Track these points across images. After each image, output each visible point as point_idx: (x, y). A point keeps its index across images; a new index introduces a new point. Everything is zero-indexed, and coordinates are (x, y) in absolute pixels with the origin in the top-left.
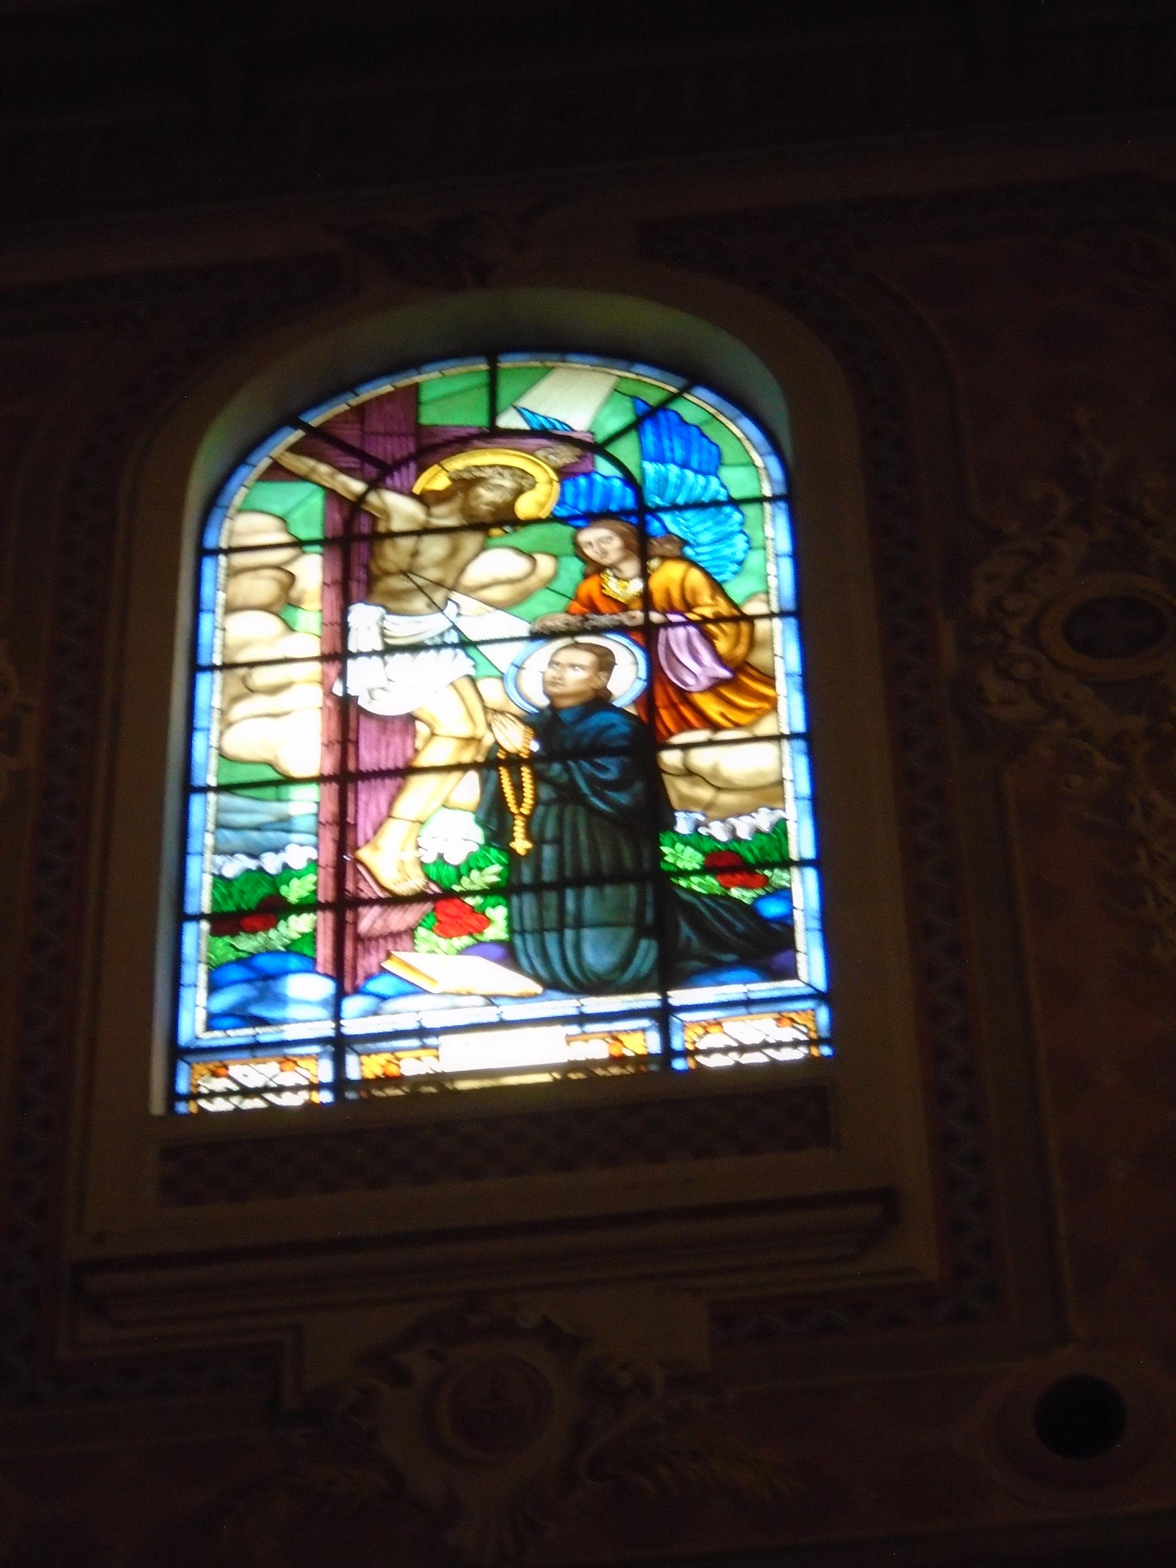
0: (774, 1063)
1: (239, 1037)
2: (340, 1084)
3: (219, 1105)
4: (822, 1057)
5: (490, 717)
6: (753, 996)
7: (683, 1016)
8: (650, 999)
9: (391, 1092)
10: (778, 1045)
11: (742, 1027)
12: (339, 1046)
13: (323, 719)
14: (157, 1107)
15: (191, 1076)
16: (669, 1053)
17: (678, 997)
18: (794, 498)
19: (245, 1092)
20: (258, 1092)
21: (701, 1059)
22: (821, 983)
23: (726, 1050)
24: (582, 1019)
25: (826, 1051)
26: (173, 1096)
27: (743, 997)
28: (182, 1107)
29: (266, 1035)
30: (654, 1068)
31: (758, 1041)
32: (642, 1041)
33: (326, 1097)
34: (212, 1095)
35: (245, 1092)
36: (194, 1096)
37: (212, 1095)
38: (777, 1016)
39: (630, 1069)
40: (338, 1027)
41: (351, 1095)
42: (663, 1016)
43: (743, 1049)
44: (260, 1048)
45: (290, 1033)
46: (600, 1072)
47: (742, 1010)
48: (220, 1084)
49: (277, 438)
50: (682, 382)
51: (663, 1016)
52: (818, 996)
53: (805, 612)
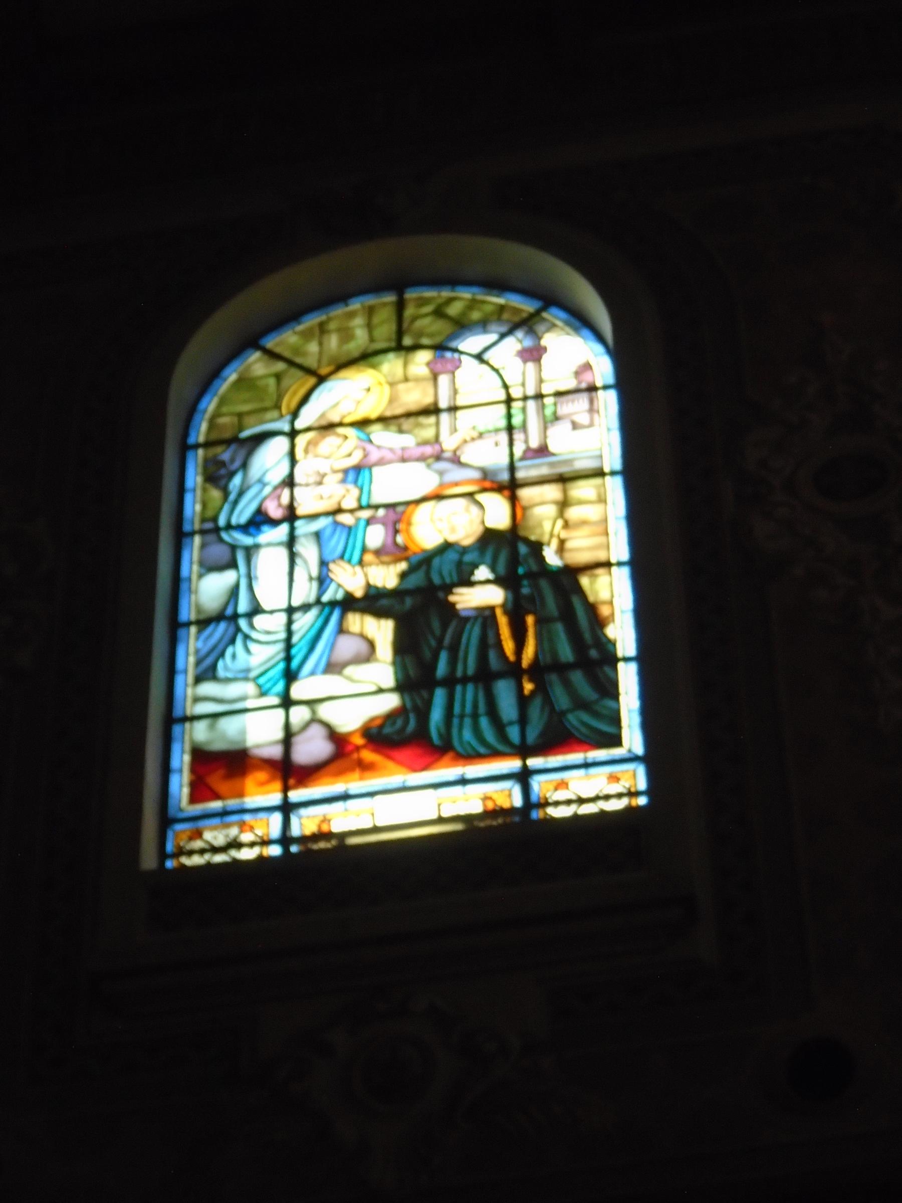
0: (603, 813)
1: (166, 770)
2: (285, 840)
3: (196, 860)
4: (639, 808)
6: (590, 761)
7: (303, 811)
8: (513, 764)
9: (322, 845)
10: (607, 797)
11: (596, 783)
13: (472, 335)
14: (149, 861)
16: (529, 804)
19: (215, 850)
22: (639, 750)
23: (569, 802)
24: (463, 781)
26: (163, 855)
27: (401, 785)
29: (232, 803)
30: (517, 819)
31: (592, 795)
33: (275, 851)
34: (557, 804)
35: (215, 850)
36: (181, 852)
37: (190, 853)
39: (500, 821)
41: (294, 849)
42: (524, 777)
43: (581, 801)
46: (476, 823)
49: (475, 290)
51: (524, 777)
52: (632, 759)
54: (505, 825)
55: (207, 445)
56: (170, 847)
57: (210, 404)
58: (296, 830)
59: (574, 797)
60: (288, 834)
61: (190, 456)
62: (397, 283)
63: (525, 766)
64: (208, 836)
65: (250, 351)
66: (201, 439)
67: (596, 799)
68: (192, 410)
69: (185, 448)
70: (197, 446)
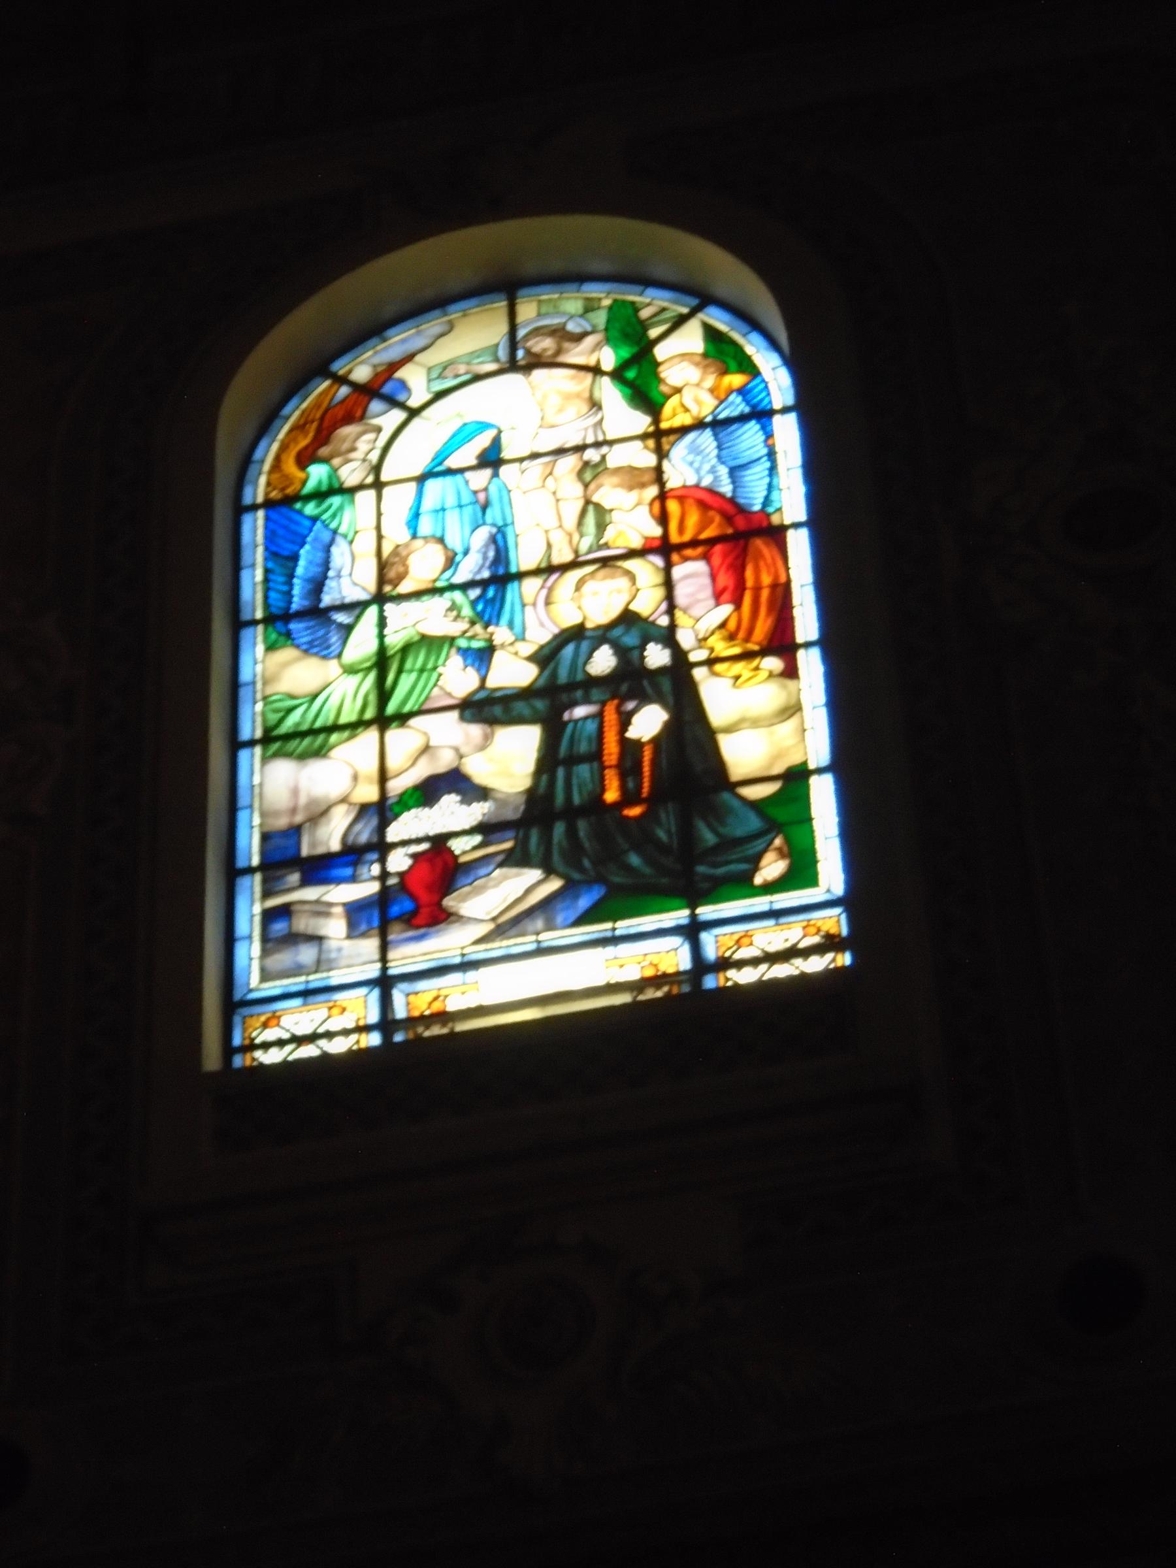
0: (325, 1057)
1: (229, 939)
2: (387, 1024)
3: (745, 977)
5: (664, 621)
6: (312, 986)
8: (681, 916)
10: (329, 1035)
12: (385, 983)
14: (212, 1060)
15: (244, 1030)
16: (701, 966)
17: (706, 912)
18: (806, 406)
20: (312, 1038)
21: (323, 1043)
25: (845, 959)
26: (229, 1051)
28: (238, 1061)
29: (316, 980)
32: (674, 956)
33: (374, 1039)
34: (266, 1046)
36: (252, 1047)
37: (266, 1046)
38: (805, 924)
40: (384, 969)
44: (313, 998)
45: (336, 977)
47: (771, 922)
48: (270, 1035)
50: (694, 302)
51: (692, 931)
53: (817, 522)
54: (668, 997)
55: (269, 504)
56: (237, 1041)
57: (268, 451)
58: (400, 1011)
59: (286, 1036)
60: (390, 1017)
61: (247, 520)
62: (506, 286)
63: (693, 916)
64: (286, 1021)
65: (318, 380)
66: (260, 499)
67: (312, 1038)
68: (245, 463)
69: (240, 510)
70: (254, 507)
